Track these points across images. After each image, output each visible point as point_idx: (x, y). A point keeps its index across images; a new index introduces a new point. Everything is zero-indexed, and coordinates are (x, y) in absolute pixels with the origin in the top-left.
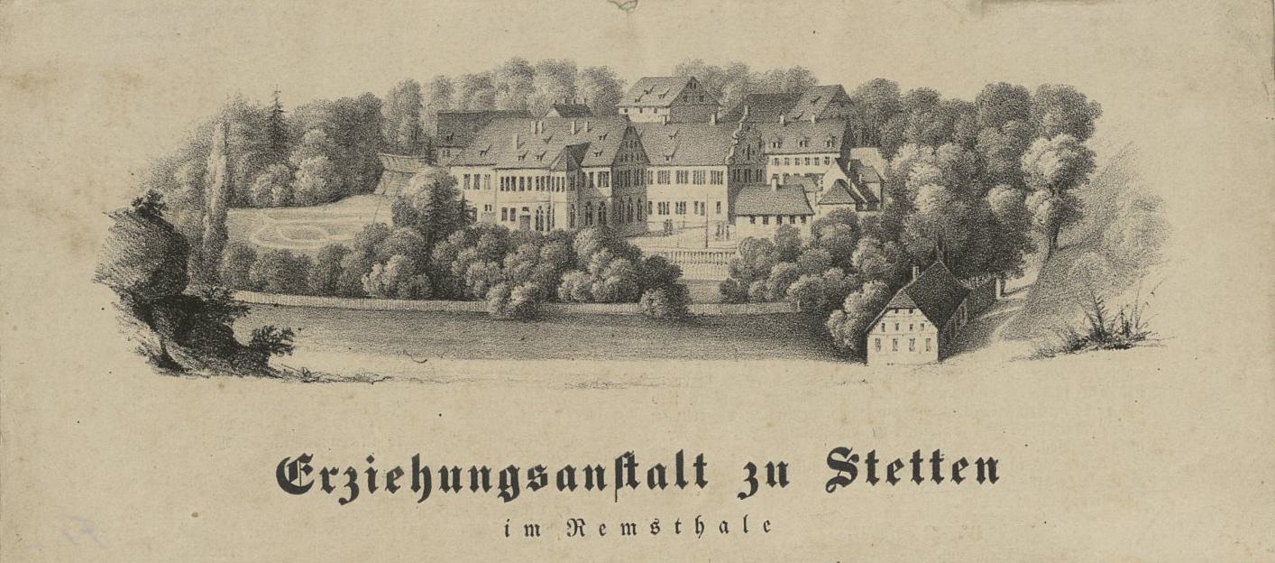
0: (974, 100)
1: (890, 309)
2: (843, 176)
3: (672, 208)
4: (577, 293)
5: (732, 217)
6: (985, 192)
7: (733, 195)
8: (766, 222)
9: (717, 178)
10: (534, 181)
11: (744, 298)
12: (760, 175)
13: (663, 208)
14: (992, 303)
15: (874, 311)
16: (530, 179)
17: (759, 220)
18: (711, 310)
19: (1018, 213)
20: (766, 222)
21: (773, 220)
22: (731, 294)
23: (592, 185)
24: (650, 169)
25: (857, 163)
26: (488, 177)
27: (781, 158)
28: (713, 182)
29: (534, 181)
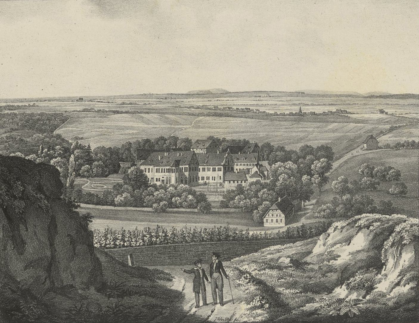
0: (276, 146)
1: (271, 210)
2: (257, 170)
3: (211, 178)
4: (179, 203)
5: (224, 181)
6: (301, 177)
7: (224, 174)
8: (234, 182)
9: (219, 170)
10: (166, 169)
11: (227, 207)
12: (232, 169)
13: (203, 178)
14: (300, 209)
15: (266, 211)
16: (164, 169)
17: (232, 182)
18: (216, 210)
19: (310, 183)
20: (234, 182)
21: (236, 182)
22: (224, 205)
23: (182, 171)
24: (199, 167)
25: (261, 165)
26: (174, 169)
27: (239, 164)
28: (218, 171)
29: (166, 169)
